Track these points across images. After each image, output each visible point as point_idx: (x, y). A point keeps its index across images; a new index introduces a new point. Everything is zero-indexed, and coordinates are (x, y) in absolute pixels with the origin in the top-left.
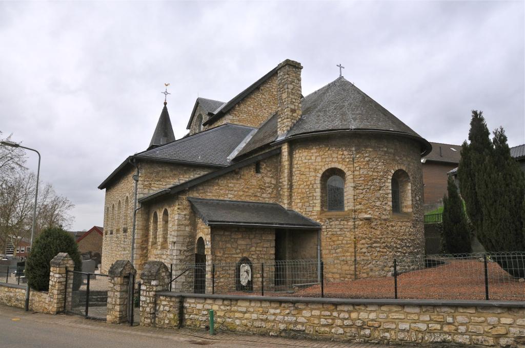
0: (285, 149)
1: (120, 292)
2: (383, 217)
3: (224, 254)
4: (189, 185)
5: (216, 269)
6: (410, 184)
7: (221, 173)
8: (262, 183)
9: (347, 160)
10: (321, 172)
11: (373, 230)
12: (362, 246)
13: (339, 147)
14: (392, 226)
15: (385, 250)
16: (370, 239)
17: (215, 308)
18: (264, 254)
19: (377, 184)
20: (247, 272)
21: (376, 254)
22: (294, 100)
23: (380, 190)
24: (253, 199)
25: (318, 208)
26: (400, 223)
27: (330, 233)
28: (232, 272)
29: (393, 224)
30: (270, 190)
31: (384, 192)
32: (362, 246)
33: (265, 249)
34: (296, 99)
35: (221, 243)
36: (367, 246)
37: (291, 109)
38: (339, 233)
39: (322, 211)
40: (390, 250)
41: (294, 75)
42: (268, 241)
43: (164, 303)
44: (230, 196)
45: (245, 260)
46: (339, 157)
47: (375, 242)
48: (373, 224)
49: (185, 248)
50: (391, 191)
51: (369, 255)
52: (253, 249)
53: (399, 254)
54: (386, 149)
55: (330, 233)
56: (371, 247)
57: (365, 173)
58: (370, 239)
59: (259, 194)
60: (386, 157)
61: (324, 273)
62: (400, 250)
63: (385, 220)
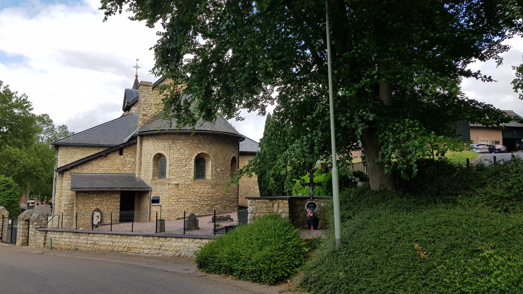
0: (138, 138)
1: (23, 229)
2: (187, 183)
3: (84, 206)
4: (70, 166)
5: (78, 215)
6: (211, 161)
7: (113, 150)
8: (124, 161)
9: (167, 148)
10: (153, 155)
11: (179, 191)
12: (172, 201)
13: (162, 140)
14: (193, 189)
15: (187, 203)
16: (178, 196)
17: (57, 236)
18: (112, 206)
19: (184, 163)
20: (98, 217)
21: (181, 205)
22: (145, 108)
23: (186, 166)
24: (117, 172)
25: (151, 178)
26: (199, 187)
27: (156, 193)
28: (89, 217)
29: (194, 187)
30: (130, 165)
31: (188, 167)
32: (172, 201)
33: (113, 203)
34: (147, 108)
35: (82, 200)
36: (175, 200)
37: (143, 114)
38: (160, 193)
39: (153, 179)
40: (191, 203)
41: (146, 91)
42: (115, 198)
43: (39, 234)
44: (100, 170)
45: (98, 210)
46: (163, 146)
47: (181, 198)
48: (180, 187)
49: (68, 203)
50: (193, 167)
51: (176, 206)
52: (104, 203)
53: (197, 205)
54: (191, 141)
55: (156, 193)
56: (178, 201)
57: (177, 156)
58: (178, 196)
59: (121, 168)
60: (192, 146)
61: (151, 217)
62: (198, 203)
63: (188, 185)
